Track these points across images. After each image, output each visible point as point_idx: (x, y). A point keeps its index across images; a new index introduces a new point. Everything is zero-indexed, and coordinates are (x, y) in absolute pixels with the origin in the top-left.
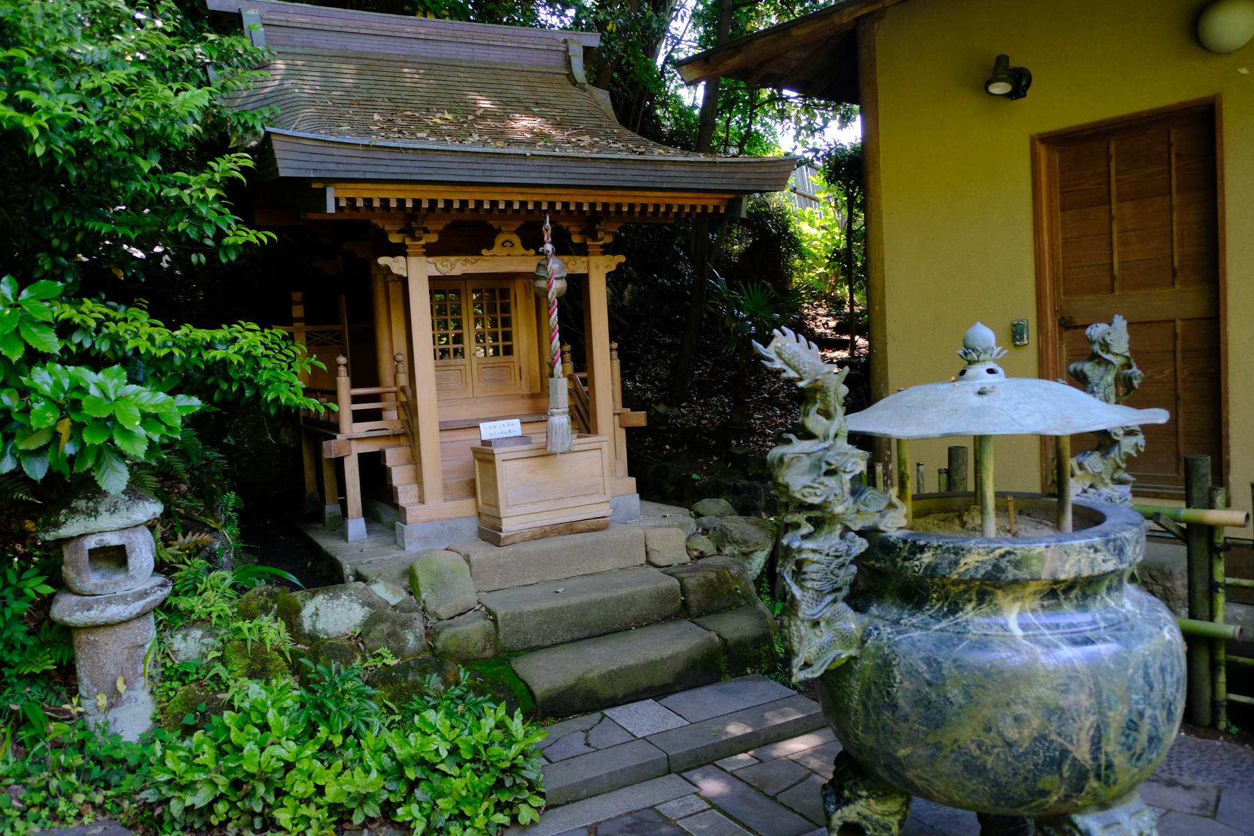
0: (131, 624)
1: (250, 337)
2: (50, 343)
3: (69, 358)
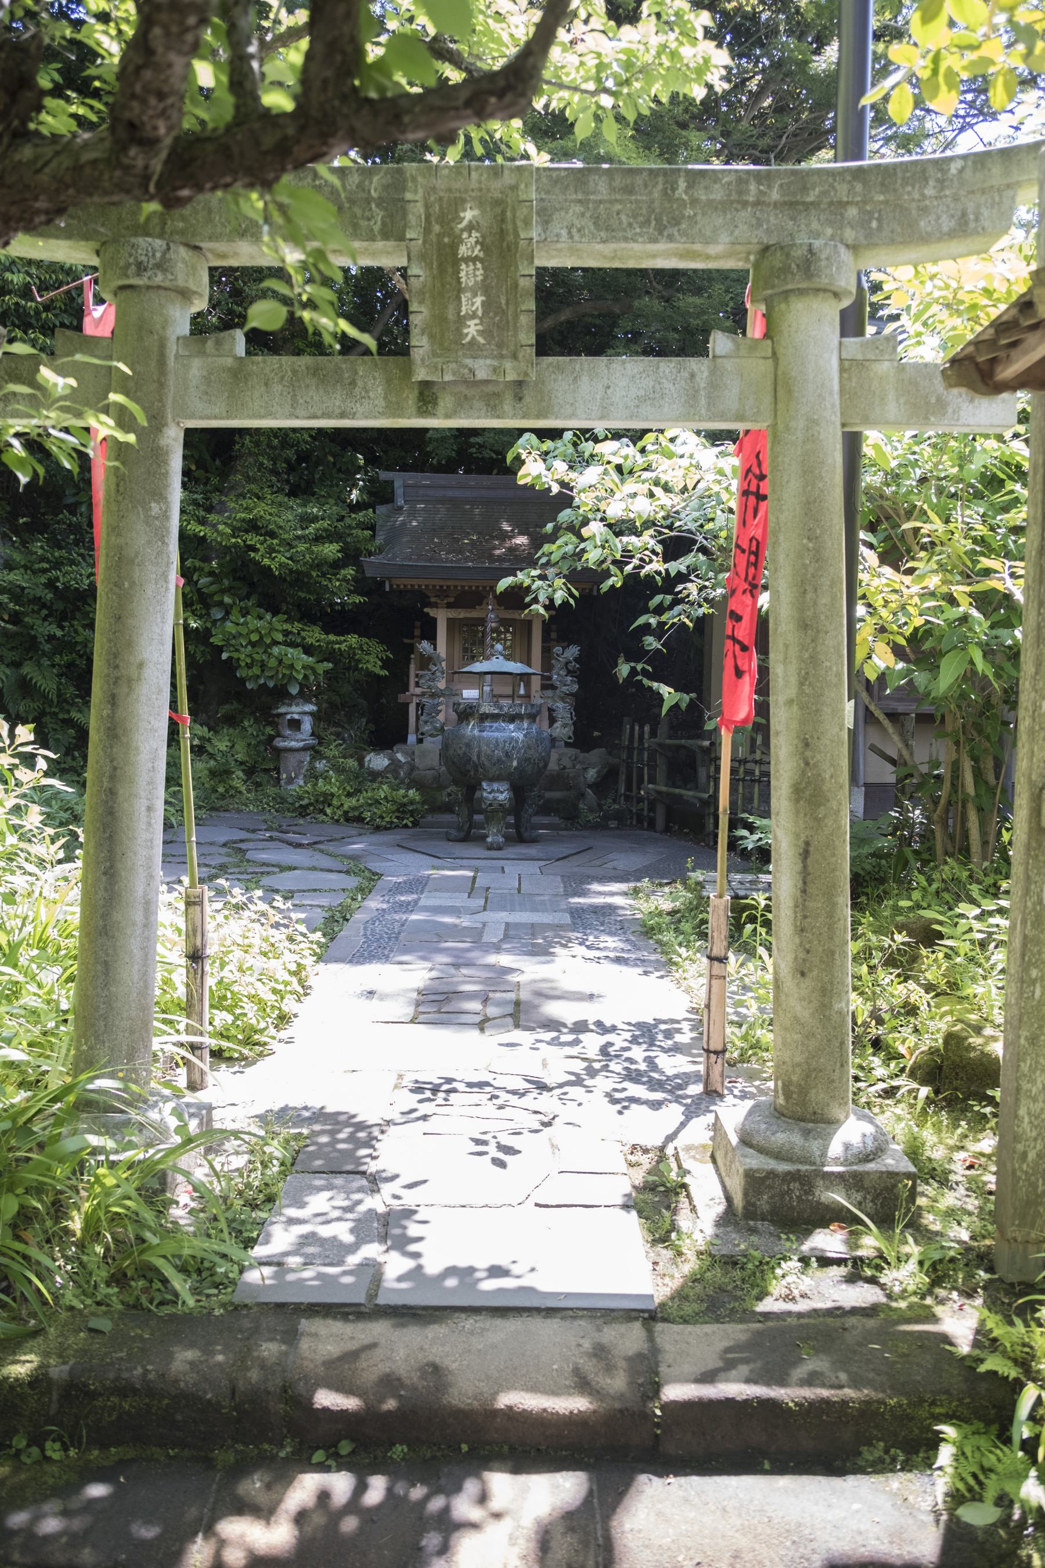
0: (810, 869)
1: (353, 639)
2: (280, 637)
3: (287, 644)
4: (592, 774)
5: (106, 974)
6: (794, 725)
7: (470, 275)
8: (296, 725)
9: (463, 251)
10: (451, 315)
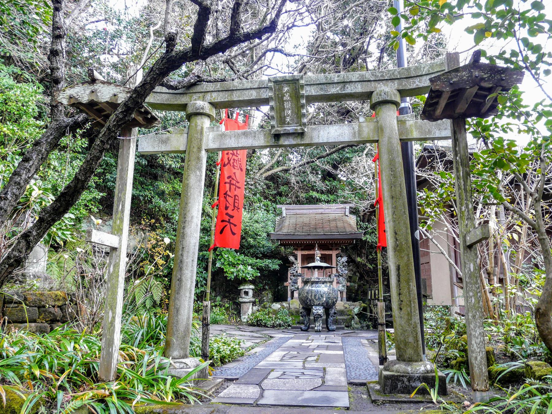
4: (356, 310)
5: (177, 312)
6: (392, 228)
7: (287, 105)
8: (246, 293)
9: (285, 98)
10: (282, 116)
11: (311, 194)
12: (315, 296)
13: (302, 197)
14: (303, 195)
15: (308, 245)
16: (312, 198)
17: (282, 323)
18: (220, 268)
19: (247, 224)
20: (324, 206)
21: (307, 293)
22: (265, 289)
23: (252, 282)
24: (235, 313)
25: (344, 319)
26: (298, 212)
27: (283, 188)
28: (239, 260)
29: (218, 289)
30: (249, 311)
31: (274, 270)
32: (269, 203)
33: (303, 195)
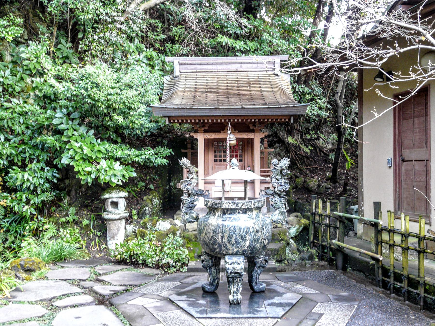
8: (115, 204)
11: (219, 40)
12: (230, 237)
13: (206, 44)
14: (207, 41)
15: (216, 125)
16: (222, 46)
17: (171, 262)
18: (68, 165)
19: (110, 91)
20: (243, 58)
21: (214, 231)
22: (147, 191)
23: (124, 186)
24: (99, 234)
25: (275, 250)
26: (199, 68)
27: (176, 30)
28: (100, 151)
29: (73, 192)
30: (119, 236)
31: (161, 166)
32: (154, 54)
33: (207, 41)
